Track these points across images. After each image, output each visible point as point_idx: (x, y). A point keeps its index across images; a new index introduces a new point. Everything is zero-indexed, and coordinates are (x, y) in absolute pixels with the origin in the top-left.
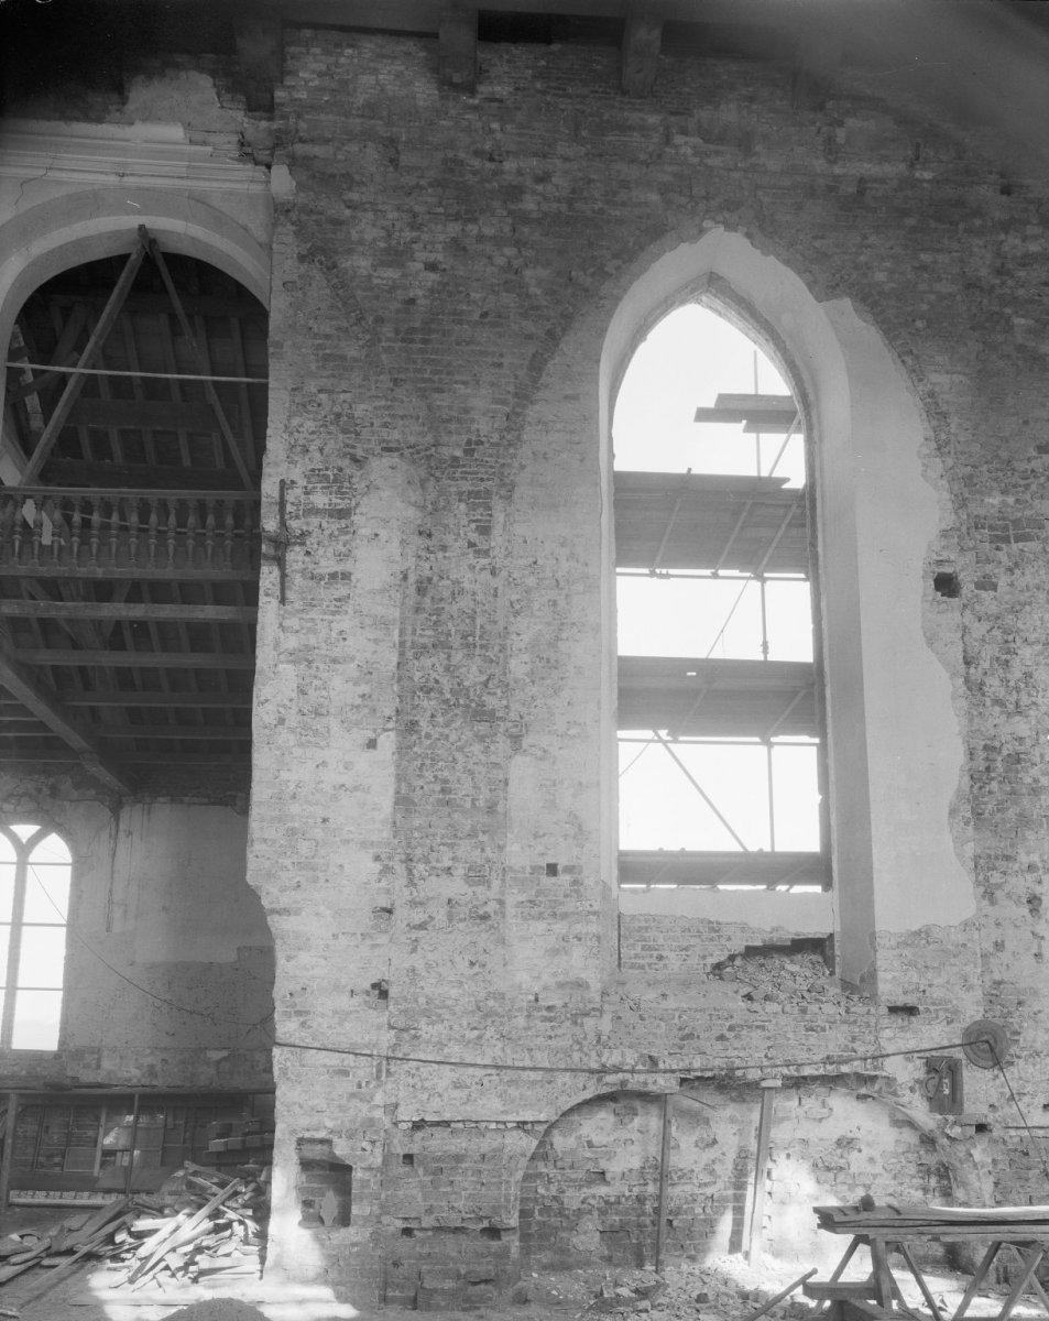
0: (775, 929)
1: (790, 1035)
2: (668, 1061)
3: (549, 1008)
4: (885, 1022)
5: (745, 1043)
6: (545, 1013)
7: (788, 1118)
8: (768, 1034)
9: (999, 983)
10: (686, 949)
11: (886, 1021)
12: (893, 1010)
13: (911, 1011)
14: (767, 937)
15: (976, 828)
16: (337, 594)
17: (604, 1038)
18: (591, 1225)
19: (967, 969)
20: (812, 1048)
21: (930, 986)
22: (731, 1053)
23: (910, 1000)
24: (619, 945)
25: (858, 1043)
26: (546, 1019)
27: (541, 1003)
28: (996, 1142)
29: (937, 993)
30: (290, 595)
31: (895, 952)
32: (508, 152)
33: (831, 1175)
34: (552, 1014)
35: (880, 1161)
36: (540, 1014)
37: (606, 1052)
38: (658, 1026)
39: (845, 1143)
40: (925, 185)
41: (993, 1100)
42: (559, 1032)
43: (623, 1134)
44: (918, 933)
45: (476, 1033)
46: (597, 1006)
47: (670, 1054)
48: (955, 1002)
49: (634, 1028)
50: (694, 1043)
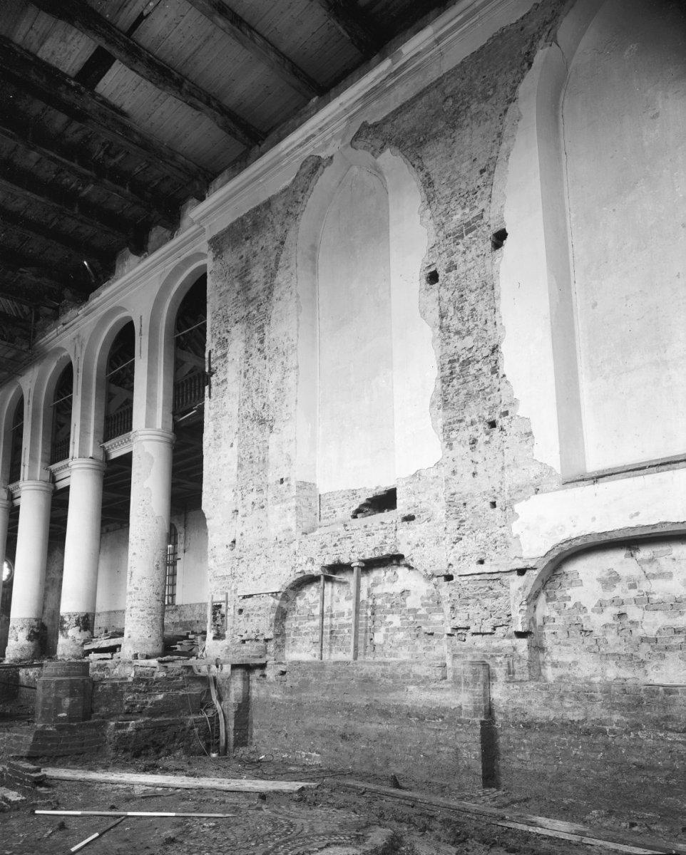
0: (377, 488)
1: (360, 539)
9: (454, 494)
10: (343, 506)
14: (374, 492)
15: (444, 410)
16: (223, 388)
23: (411, 512)
29: (423, 506)
30: (212, 395)
32: (385, 144)
40: (210, 175)
44: (414, 475)
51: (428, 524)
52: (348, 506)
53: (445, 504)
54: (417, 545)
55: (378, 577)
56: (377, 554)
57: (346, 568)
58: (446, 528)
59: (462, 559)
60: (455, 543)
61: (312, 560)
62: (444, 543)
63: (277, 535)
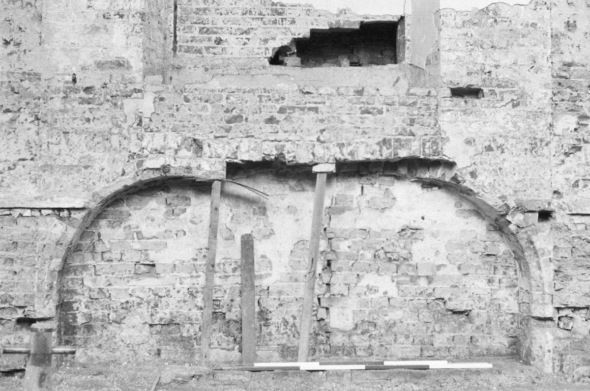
0: (343, 12)
1: (345, 118)
2: (214, 145)
3: (87, 90)
4: (448, 103)
5: (296, 126)
6: (82, 94)
7: (350, 209)
8: (320, 116)
9: (570, 65)
10: (246, 32)
11: (448, 103)
12: (457, 92)
13: (474, 92)
17: (145, 121)
18: (137, 319)
19: (537, 49)
20: (366, 130)
21: (497, 67)
22: (281, 136)
23: (475, 81)
24: (175, 28)
25: (416, 126)
26: (83, 101)
27: (79, 84)
28: (558, 228)
29: (504, 74)
31: (459, 31)
33: (393, 266)
34: (91, 96)
35: (443, 252)
36: (78, 96)
37: (148, 136)
38: (204, 107)
39: (410, 232)
41: (556, 186)
42: (98, 114)
43: (172, 225)
44: (485, 11)
45: (10, 115)
46: (138, 87)
47: (216, 137)
48: (521, 85)
49: (178, 110)
50: (243, 126)
51: (513, 112)
52: (260, 33)
53: (550, 80)
54: (489, 149)
55: (346, 197)
56: (386, 154)
57: (300, 174)
58: (551, 125)
59: (581, 183)
60: (567, 154)
61: (197, 146)
62: (546, 151)
63: (74, 70)
